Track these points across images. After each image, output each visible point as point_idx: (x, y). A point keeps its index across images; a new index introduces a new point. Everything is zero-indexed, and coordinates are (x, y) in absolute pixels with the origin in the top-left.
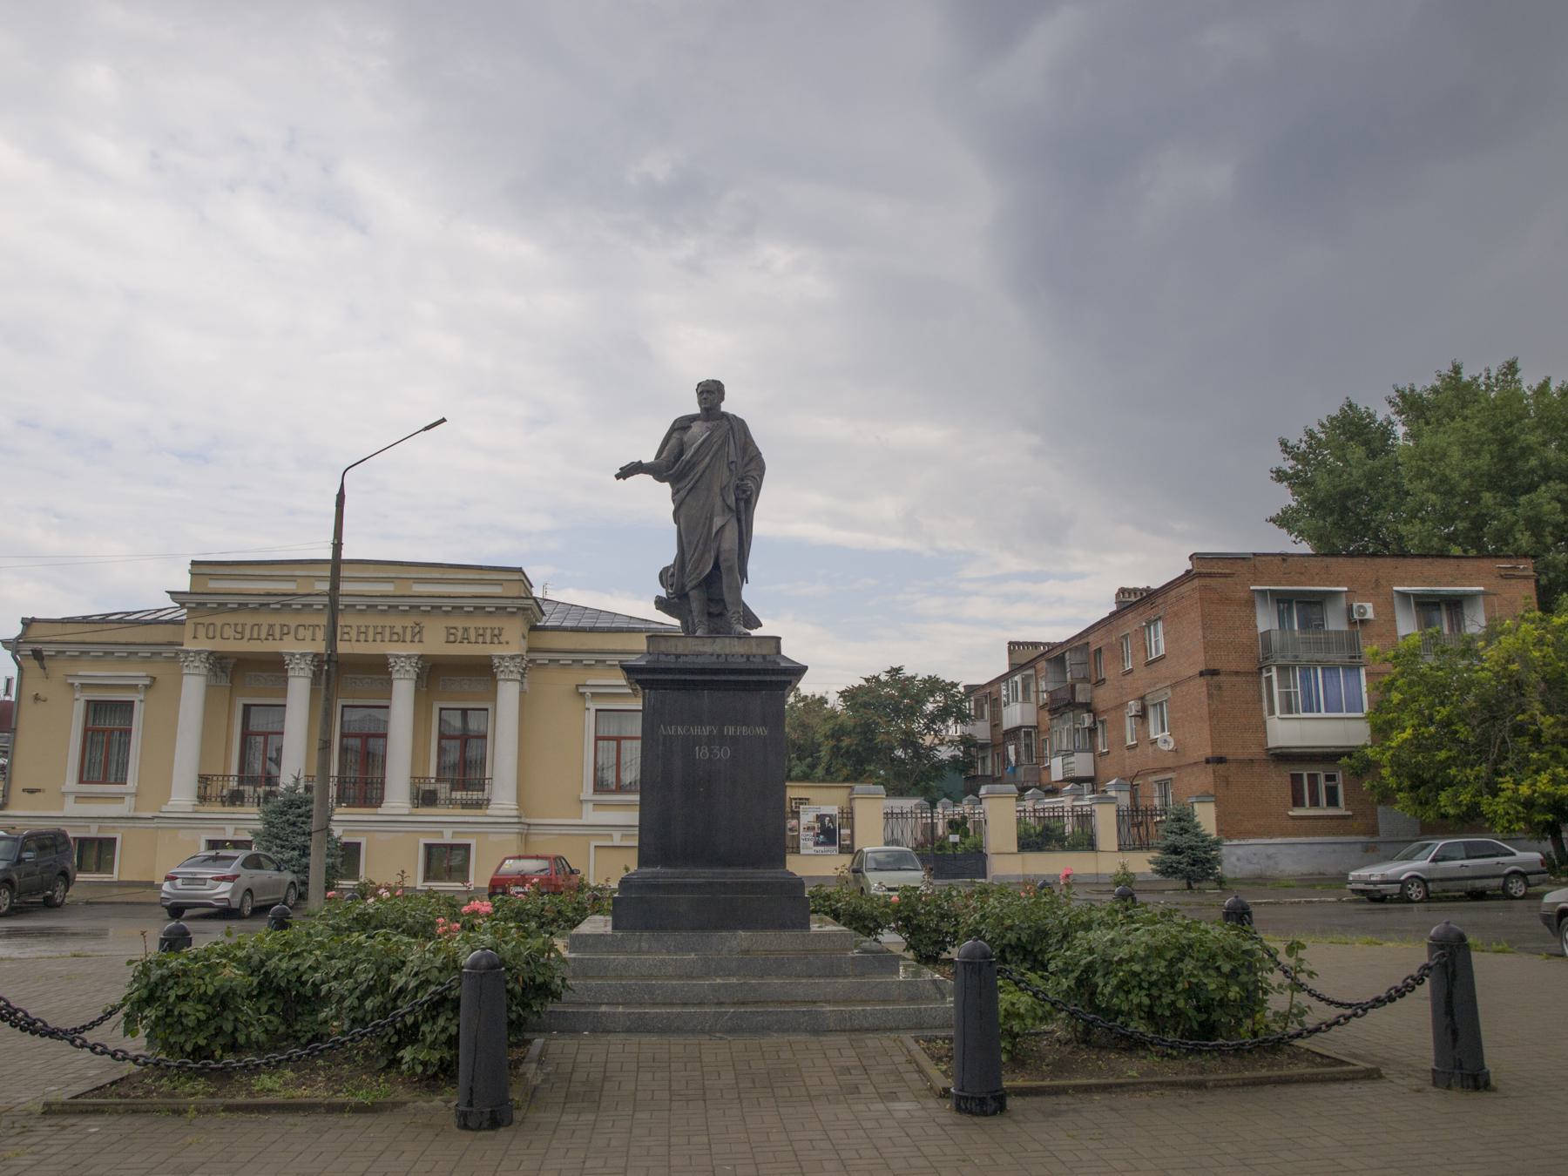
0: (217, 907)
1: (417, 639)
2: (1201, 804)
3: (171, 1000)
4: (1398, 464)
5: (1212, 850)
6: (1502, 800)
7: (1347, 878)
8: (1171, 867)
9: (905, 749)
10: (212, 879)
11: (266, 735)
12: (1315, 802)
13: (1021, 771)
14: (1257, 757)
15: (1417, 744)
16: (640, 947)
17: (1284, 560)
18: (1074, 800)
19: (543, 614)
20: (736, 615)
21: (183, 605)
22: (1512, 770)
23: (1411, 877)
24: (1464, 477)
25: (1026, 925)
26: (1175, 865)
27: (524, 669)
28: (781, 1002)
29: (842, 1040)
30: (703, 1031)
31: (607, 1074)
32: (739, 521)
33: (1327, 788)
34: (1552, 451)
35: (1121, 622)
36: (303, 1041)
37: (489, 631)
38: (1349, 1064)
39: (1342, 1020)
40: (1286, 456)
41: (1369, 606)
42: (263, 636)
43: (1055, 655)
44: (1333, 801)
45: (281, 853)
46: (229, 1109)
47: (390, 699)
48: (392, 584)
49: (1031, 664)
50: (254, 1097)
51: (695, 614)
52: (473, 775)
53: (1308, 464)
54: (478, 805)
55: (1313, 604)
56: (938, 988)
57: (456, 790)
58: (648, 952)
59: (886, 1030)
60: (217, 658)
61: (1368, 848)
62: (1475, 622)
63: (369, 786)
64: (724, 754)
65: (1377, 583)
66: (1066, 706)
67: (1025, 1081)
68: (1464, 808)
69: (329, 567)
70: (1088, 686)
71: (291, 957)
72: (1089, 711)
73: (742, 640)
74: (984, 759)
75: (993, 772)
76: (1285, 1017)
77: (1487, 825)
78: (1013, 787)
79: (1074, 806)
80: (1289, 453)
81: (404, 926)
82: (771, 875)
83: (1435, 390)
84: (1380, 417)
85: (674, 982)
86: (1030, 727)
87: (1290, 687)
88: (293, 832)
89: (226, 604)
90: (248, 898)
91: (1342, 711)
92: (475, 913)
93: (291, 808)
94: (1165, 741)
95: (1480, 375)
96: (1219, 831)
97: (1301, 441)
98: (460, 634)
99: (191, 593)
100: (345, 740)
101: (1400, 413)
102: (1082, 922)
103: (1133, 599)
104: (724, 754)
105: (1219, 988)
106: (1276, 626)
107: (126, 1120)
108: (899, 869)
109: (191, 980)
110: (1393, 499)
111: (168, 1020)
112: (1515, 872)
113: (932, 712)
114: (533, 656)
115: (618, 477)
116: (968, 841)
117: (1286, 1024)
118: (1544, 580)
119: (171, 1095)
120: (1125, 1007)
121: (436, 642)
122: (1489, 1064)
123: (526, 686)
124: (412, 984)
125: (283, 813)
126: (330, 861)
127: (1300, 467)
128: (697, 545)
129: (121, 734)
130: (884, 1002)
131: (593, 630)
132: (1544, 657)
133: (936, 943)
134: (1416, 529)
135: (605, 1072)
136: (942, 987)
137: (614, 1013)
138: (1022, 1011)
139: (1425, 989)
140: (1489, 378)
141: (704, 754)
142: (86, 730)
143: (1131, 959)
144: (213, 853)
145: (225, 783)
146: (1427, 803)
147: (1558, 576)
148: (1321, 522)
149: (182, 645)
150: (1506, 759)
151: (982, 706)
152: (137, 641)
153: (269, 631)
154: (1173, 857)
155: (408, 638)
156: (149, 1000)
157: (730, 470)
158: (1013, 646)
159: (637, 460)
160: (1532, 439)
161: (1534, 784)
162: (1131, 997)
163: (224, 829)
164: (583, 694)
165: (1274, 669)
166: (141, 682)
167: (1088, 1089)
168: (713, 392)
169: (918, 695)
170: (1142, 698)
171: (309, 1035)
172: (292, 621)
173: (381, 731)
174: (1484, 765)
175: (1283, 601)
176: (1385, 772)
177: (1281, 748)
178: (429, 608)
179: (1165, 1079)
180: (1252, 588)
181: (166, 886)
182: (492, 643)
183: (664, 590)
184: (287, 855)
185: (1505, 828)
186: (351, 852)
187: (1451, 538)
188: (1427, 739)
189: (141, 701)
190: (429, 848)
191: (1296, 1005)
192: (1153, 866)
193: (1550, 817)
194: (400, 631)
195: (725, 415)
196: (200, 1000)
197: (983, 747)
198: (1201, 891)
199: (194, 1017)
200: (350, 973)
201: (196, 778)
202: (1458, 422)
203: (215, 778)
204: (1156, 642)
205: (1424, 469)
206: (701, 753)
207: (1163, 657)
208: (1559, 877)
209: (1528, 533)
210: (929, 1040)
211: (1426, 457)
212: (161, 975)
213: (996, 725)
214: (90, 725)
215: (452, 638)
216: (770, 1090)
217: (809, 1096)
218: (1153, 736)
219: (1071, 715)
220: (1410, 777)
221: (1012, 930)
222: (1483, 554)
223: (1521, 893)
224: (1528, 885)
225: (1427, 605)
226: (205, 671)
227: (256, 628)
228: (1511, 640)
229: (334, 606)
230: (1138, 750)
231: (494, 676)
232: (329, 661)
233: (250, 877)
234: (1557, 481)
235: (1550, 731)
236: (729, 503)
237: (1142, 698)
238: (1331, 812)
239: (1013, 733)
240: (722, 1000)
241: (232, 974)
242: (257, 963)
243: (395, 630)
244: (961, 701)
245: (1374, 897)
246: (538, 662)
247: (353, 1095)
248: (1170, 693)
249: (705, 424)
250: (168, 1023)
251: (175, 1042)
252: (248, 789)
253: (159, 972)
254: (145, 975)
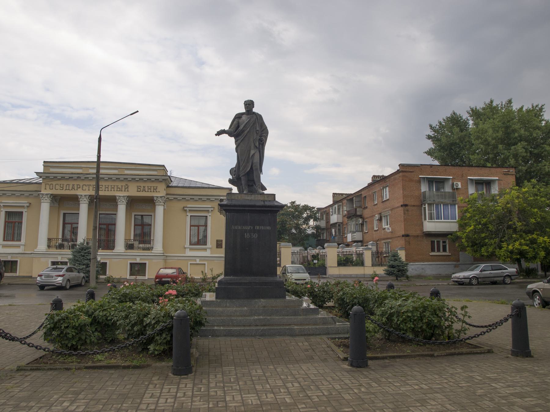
0: (57, 286)
1: (126, 190)
3: (63, 328)
4: (470, 134)
6: (503, 251)
7: (451, 276)
8: (391, 272)
9: (296, 229)
10: (55, 276)
11: (72, 224)
12: (439, 250)
13: (336, 238)
14: (420, 235)
15: (474, 231)
17: (431, 167)
18: (356, 249)
19: (172, 182)
21: (41, 177)
22: (506, 241)
23: (473, 277)
24: (493, 139)
25: (361, 297)
26: (392, 272)
27: (165, 201)
29: (302, 338)
30: (252, 336)
33: (443, 246)
34: (522, 131)
35: (373, 187)
36: (109, 341)
37: (152, 188)
38: (481, 347)
39: (483, 333)
40: (431, 130)
41: (459, 183)
42: (70, 188)
43: (349, 198)
44: (444, 250)
45: (79, 266)
46: (87, 368)
47: (117, 211)
48: (117, 170)
49: (341, 201)
50: (95, 363)
52: (147, 238)
53: (439, 133)
54: (148, 249)
55: (441, 182)
56: (334, 320)
57: (141, 244)
58: (228, 307)
59: (316, 335)
60: (53, 196)
61: (456, 266)
62: (495, 190)
63: (109, 242)
64: (255, 236)
65: (462, 176)
66: (353, 216)
68: (490, 253)
70: (361, 209)
71: (103, 311)
72: (361, 218)
73: (262, 195)
74: (323, 233)
75: (326, 238)
76: (459, 331)
77: (497, 259)
78: (336, 244)
80: (432, 129)
82: (272, 279)
83: (484, 109)
84: (464, 118)
85: (241, 318)
86: (340, 223)
87: (432, 211)
88: (83, 259)
89: (57, 177)
90: (68, 282)
91: (449, 219)
92: (171, 294)
94: (388, 229)
95: (499, 104)
97: (437, 125)
98: (142, 189)
99: (43, 173)
100: (100, 226)
101: (471, 116)
103: (378, 179)
104: (255, 236)
105: (438, 322)
108: (299, 273)
109: (70, 321)
110: (468, 146)
111: (61, 335)
112: (508, 275)
114: (168, 196)
115: (216, 135)
117: (460, 334)
118: (518, 176)
119: (64, 363)
120: (405, 328)
121: (133, 191)
122: (531, 347)
124: (153, 322)
125: (79, 252)
126: (97, 269)
127: (436, 134)
128: (244, 160)
129: (18, 223)
130: (314, 324)
132: (519, 202)
134: (476, 157)
135: (221, 352)
137: (220, 329)
138: (371, 330)
139: (510, 320)
140: (502, 105)
141: (248, 236)
142: (5, 222)
143: (407, 312)
144: (55, 266)
145: (57, 241)
146: (477, 251)
147: (522, 175)
148: (443, 154)
149: (41, 192)
150: (505, 237)
151: (323, 215)
152: (24, 190)
154: (392, 269)
155: (123, 190)
156: (53, 329)
158: (334, 194)
159: (223, 129)
160: (517, 127)
161: (514, 245)
162: (407, 324)
164: (186, 210)
166: (25, 205)
167: (394, 357)
168: (250, 105)
170: (380, 214)
171: (111, 339)
172: (81, 183)
174: (497, 239)
175: (430, 181)
176: (463, 240)
177: (428, 232)
180: (420, 176)
181: (39, 279)
183: (231, 176)
184: (81, 267)
185: (503, 260)
186: (104, 265)
187: (487, 160)
188: (478, 229)
189: (26, 212)
191: (463, 327)
192: (385, 272)
193: (518, 257)
194: (120, 187)
195: (254, 113)
196: (73, 328)
197: (323, 229)
198: (401, 281)
200: (127, 317)
201: (47, 240)
202: (492, 120)
203: (54, 239)
204: (386, 194)
205: (479, 136)
206: (247, 236)
207: (388, 200)
208: (520, 277)
209: (513, 159)
210: (332, 339)
211: (480, 132)
212: (59, 319)
214: (7, 220)
215: (139, 190)
218: (384, 227)
220: (472, 242)
221: (356, 299)
222: (499, 166)
223: (509, 282)
224: (511, 279)
225: (478, 183)
226: (49, 201)
227: (68, 186)
228: (508, 196)
229: (98, 178)
232: (96, 198)
234: (524, 142)
235: (520, 227)
236: (256, 145)
237: (380, 214)
238: (444, 254)
239: (334, 225)
240: (258, 324)
241: (84, 318)
243: (119, 187)
244: (316, 213)
245: (460, 283)
246: (170, 198)
249: (247, 116)
250: (62, 336)
251: (64, 343)
252: (66, 243)
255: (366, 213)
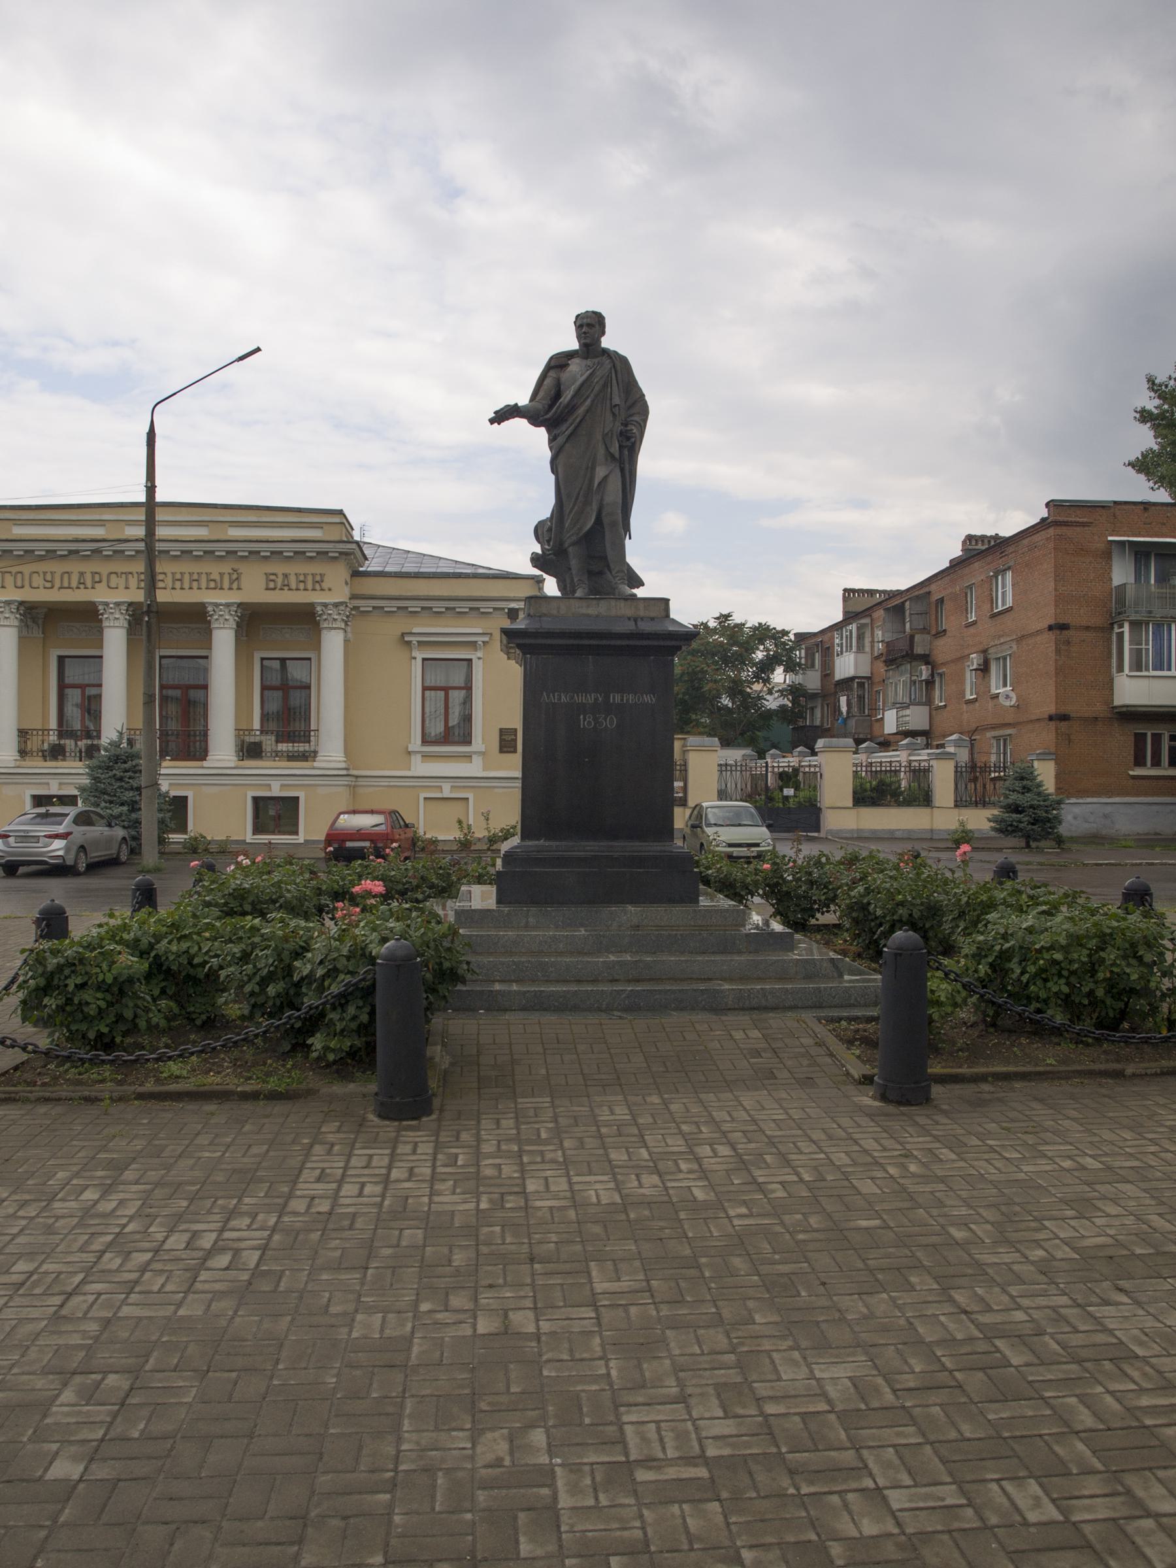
1: (235, 586)
2: (1042, 762)
3: (71, 988)
5: (1054, 809)
8: (1011, 825)
9: (732, 697)
10: (45, 836)
11: (82, 687)
13: (852, 723)
14: (1102, 715)
16: (527, 922)
17: (1146, 509)
19: (366, 559)
20: (620, 574)
25: (918, 901)
26: (1015, 823)
27: (347, 617)
28: (675, 980)
29: (744, 1019)
30: (600, 1010)
31: (515, 1057)
32: (622, 470)
35: (966, 571)
36: (198, 1022)
37: (310, 578)
40: (1152, 394)
42: (74, 584)
45: (110, 808)
46: (141, 1096)
49: (867, 612)
50: (163, 1084)
51: (574, 572)
54: (304, 757)
57: (282, 742)
60: (27, 608)
63: (192, 738)
64: (610, 723)
66: (903, 657)
67: (943, 1067)
69: (144, 509)
70: (928, 637)
71: (179, 939)
72: (927, 663)
73: (629, 602)
74: (812, 709)
79: (910, 762)
80: (1155, 391)
81: (282, 900)
87: (1141, 644)
93: (117, 763)
94: (1007, 697)
96: (1058, 789)
98: (280, 581)
100: (164, 692)
102: (982, 901)
103: (980, 547)
104: (610, 723)
106: (1132, 580)
107: (42, 1109)
108: (740, 825)
109: (88, 968)
111: (68, 1008)
113: (761, 661)
114: (357, 603)
115: (492, 421)
116: (802, 794)
123: (350, 635)
124: (320, 972)
127: (1166, 407)
130: (781, 979)
131: (418, 576)
133: (804, 910)
136: (840, 966)
137: (510, 992)
138: (943, 999)
143: (1051, 948)
144: (42, 810)
145: (46, 738)
151: (814, 655)
153: (80, 579)
154: (1014, 816)
155: (226, 584)
157: (614, 415)
158: (848, 593)
162: (1049, 984)
163: (48, 784)
164: (409, 643)
165: (1126, 628)
169: (747, 642)
170: (985, 651)
171: (204, 1017)
172: (104, 569)
173: (202, 682)
175: (1141, 554)
177: (1128, 706)
178: (247, 554)
179: (1082, 1067)
180: (1110, 538)
182: (314, 589)
184: (117, 810)
186: (180, 804)
190: (256, 800)
192: (992, 824)
194: (218, 578)
195: (605, 352)
196: (99, 988)
197: (814, 696)
199: (94, 1006)
201: (16, 733)
203: (35, 732)
207: (1010, 609)
210: (831, 1020)
213: (827, 675)
215: (272, 585)
216: (684, 1074)
217: (726, 1081)
218: (994, 691)
219: (908, 666)
226: (16, 623)
227: (66, 576)
229: (150, 551)
230: (977, 704)
231: (317, 624)
232: (148, 612)
233: (83, 833)
236: (612, 450)
239: (847, 683)
240: (617, 977)
241: (127, 961)
242: (146, 946)
243: (212, 577)
244: (792, 649)
246: (362, 609)
247: (264, 1082)
248: (1015, 647)
249: (585, 362)
250: (70, 1011)
251: (77, 1030)
252: (69, 743)
253: (55, 961)
254: (40, 963)
255: (943, 649)
